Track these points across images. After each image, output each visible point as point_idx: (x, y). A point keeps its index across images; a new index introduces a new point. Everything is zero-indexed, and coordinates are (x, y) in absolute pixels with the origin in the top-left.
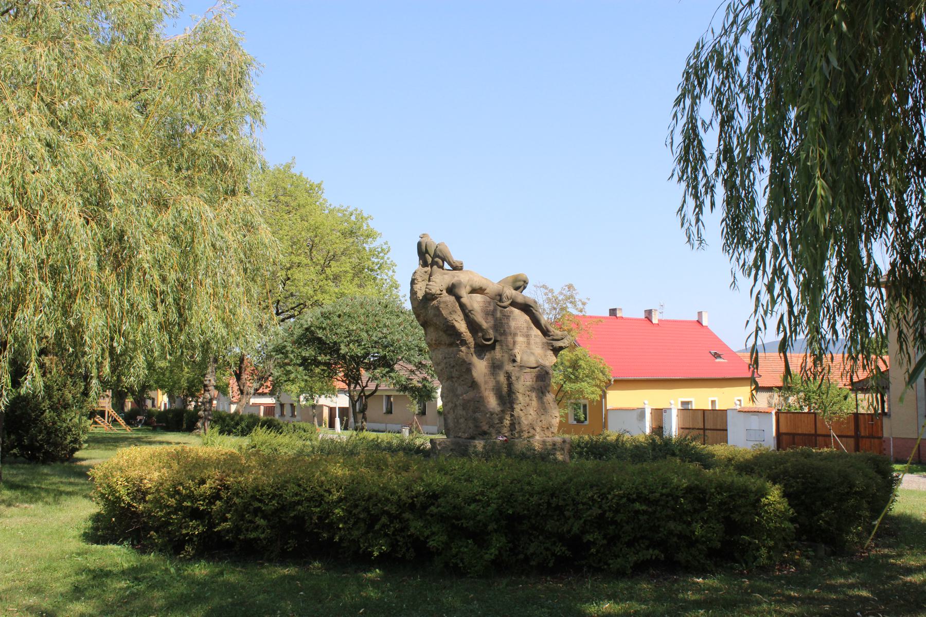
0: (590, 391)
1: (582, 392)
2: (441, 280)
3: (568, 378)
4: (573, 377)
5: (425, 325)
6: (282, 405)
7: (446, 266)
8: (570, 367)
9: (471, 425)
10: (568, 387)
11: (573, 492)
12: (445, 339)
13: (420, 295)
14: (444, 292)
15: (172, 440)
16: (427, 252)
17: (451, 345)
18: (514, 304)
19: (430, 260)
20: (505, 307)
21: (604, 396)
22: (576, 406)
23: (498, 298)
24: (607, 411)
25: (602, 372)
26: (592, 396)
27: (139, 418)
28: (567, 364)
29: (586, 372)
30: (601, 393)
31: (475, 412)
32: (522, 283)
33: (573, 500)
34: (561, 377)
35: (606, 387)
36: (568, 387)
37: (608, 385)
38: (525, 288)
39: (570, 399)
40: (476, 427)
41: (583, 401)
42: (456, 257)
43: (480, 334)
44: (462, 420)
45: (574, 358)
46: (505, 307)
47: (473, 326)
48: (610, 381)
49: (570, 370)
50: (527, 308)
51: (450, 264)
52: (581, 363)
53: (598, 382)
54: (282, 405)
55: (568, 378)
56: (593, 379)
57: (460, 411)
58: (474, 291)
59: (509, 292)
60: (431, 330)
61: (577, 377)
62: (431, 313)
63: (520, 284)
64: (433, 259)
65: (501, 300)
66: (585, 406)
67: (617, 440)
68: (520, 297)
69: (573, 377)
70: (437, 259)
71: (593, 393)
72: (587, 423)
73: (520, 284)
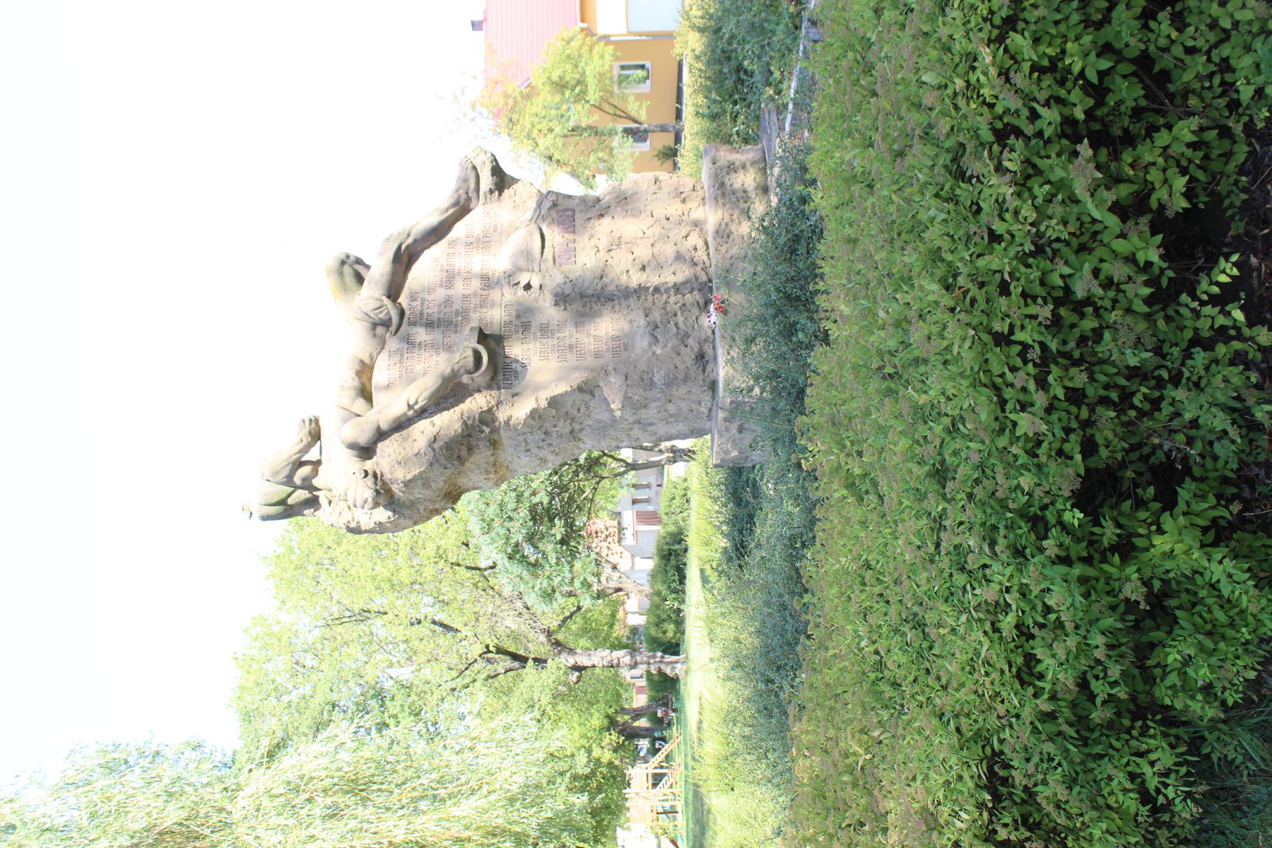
0: (600, 63)
1: (600, 74)
2: (341, 476)
3: (581, 97)
4: (577, 90)
5: (452, 496)
6: (634, 502)
7: (312, 455)
8: (563, 94)
9: (683, 390)
10: (593, 96)
11: (999, 260)
12: (482, 456)
13: (382, 515)
14: (369, 465)
15: (696, 709)
16: (282, 502)
17: (494, 444)
18: (393, 290)
19: (302, 495)
20: (402, 314)
21: (606, 39)
22: (622, 80)
23: (380, 330)
24: (629, 33)
25: (568, 42)
26: (608, 57)
27: (659, 715)
28: (558, 98)
29: (569, 67)
30: (602, 44)
31: (652, 384)
32: (347, 269)
33: (1023, 258)
34: (579, 107)
35: (593, 35)
36: (593, 96)
37: (589, 32)
38: (359, 261)
39: (612, 93)
40: (686, 379)
41: (616, 71)
42: (289, 442)
43: (465, 379)
44: (671, 408)
45: (548, 88)
46: (402, 314)
47: (449, 393)
48: (582, 30)
49: (567, 93)
50: (405, 258)
51: (306, 450)
52: (555, 77)
53: (586, 48)
54: (634, 502)
55: (581, 97)
56: (580, 56)
57: (651, 413)
58: (365, 394)
59: (371, 295)
60: (463, 481)
61: (579, 82)
62: (418, 493)
63: (352, 271)
64: (297, 488)
65: (386, 324)
66: (623, 68)
67: (701, 30)
68: (380, 267)
69: (577, 90)
70: (297, 479)
71: (602, 57)
72: (648, 64)
73: (352, 271)
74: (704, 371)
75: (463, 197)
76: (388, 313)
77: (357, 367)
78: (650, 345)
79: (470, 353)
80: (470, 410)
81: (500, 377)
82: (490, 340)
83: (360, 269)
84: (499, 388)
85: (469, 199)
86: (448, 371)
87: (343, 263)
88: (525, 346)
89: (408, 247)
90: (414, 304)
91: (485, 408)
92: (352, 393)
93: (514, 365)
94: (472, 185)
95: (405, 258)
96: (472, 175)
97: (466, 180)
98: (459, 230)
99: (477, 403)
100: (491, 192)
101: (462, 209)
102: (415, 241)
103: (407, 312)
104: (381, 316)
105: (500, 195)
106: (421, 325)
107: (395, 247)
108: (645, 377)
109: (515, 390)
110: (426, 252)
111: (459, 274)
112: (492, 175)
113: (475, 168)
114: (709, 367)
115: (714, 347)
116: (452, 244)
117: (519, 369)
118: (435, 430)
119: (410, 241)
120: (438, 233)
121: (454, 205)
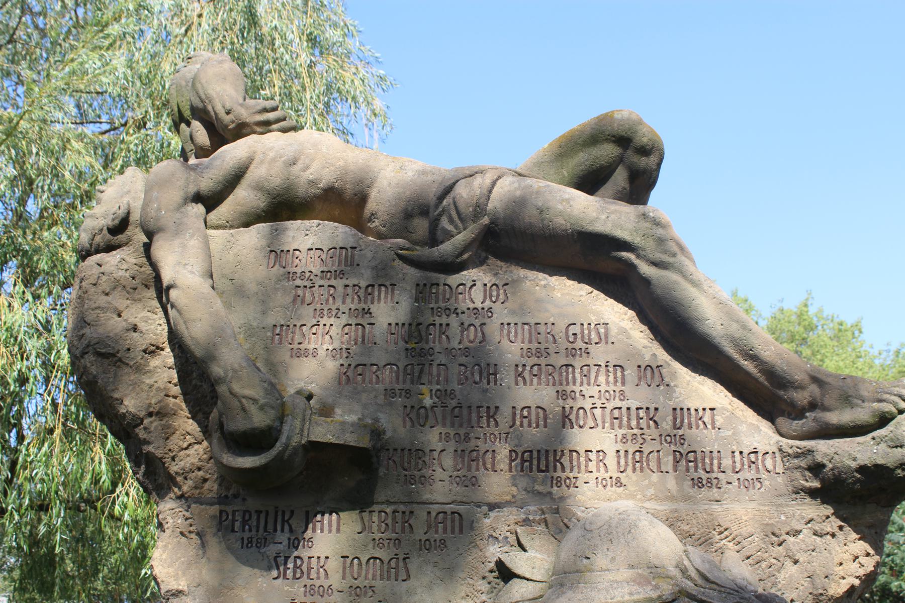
23: (421, 226)
32: (608, 151)
43: (214, 415)
63: (621, 160)
75: (801, 397)
76: (449, 235)
77: (349, 189)
79: (259, 419)
80: (168, 433)
81: (253, 504)
82: (346, 475)
83: (620, 178)
84: (222, 500)
85: (797, 413)
86: (217, 370)
87: (624, 140)
88: (334, 565)
89: (632, 267)
91: (174, 468)
92: (276, 181)
93: (283, 538)
94: (835, 418)
95: (599, 262)
96: (861, 414)
97: (848, 393)
98: (702, 392)
99: (188, 447)
100: (816, 469)
101: (765, 391)
102: (646, 282)
103: (453, 280)
104: (445, 223)
105: (812, 493)
106: (416, 312)
107: (624, 235)
109: (213, 542)
110: (631, 313)
111: (562, 395)
112: (862, 469)
113: (884, 420)
116: (651, 373)
117: (272, 550)
118: (137, 356)
119: (645, 269)
120: (682, 337)
121: (770, 372)
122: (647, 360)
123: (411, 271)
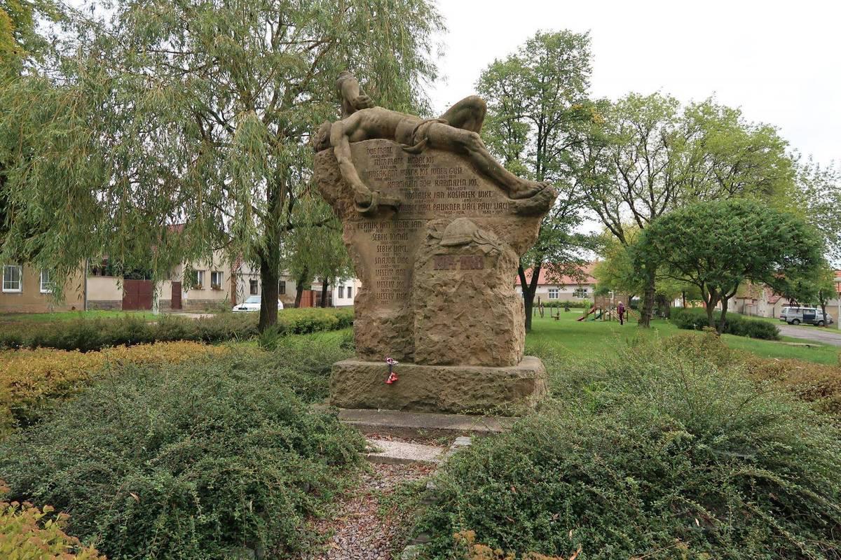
74: (362, 352)
75: (515, 187)
76: (417, 143)
78: (380, 318)
90: (425, 160)
103: (418, 156)
105: (515, 214)
108: (358, 314)
114: (365, 357)
115: (378, 361)
122: (472, 178)
123: (406, 154)
